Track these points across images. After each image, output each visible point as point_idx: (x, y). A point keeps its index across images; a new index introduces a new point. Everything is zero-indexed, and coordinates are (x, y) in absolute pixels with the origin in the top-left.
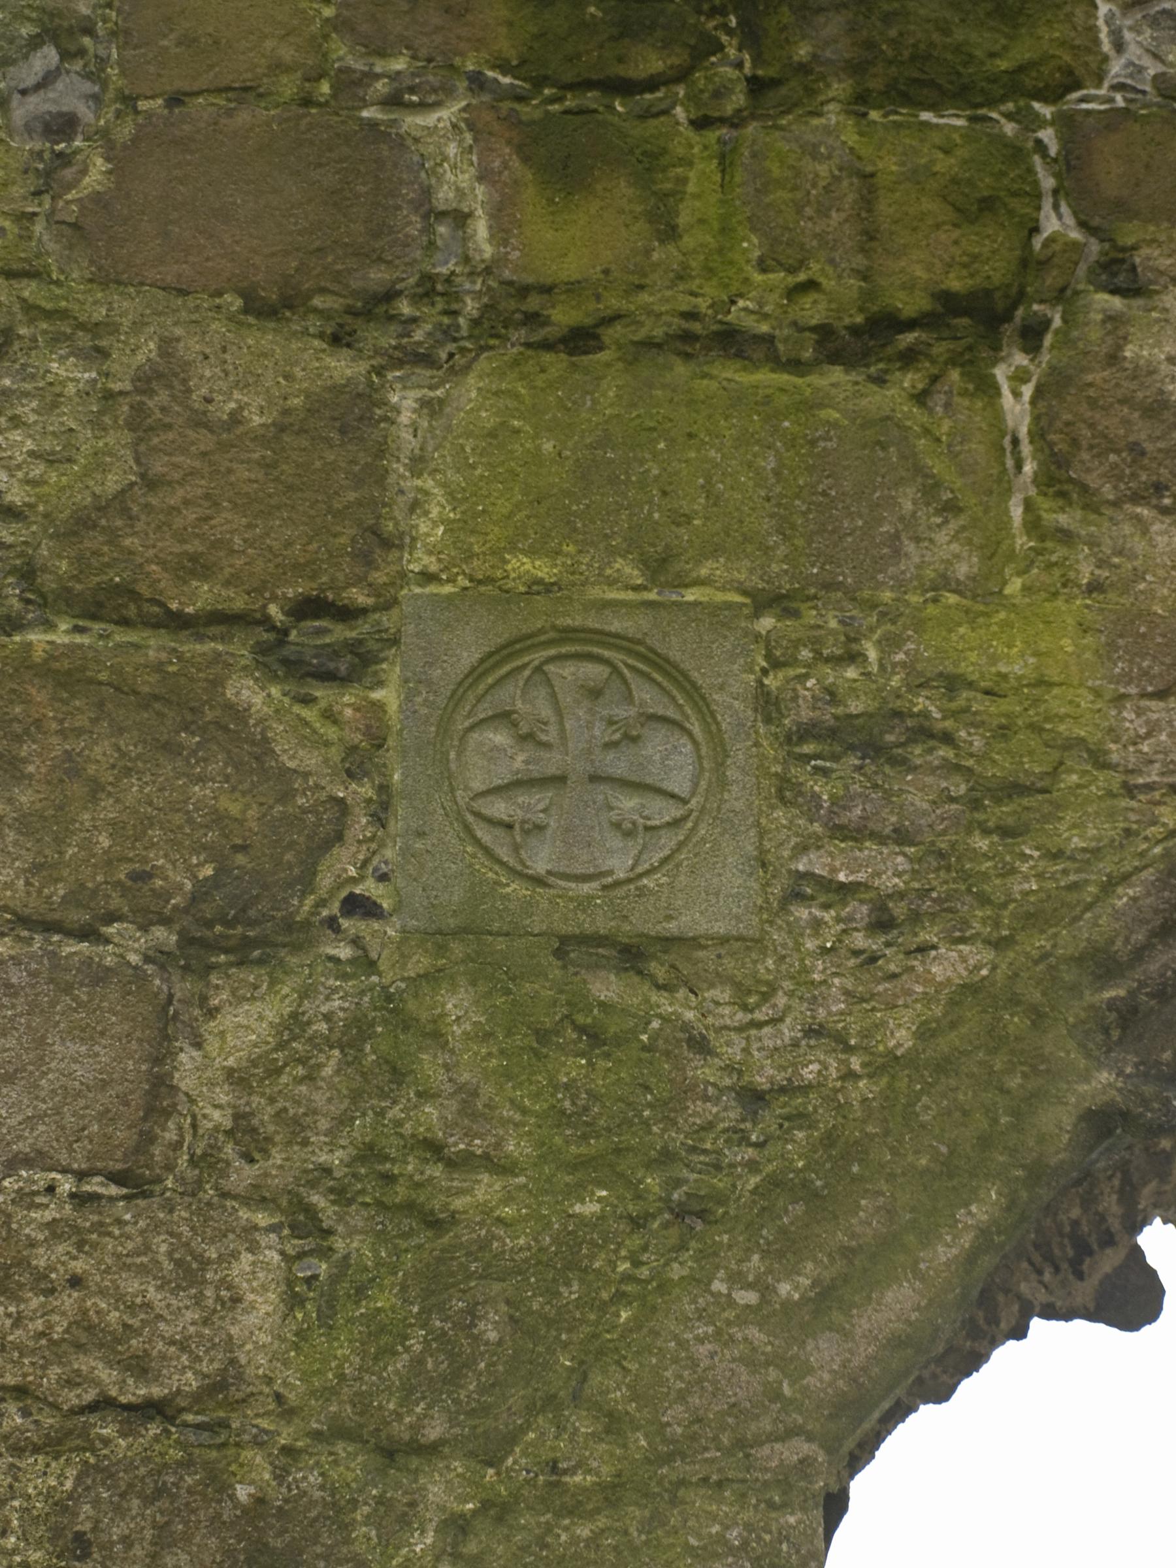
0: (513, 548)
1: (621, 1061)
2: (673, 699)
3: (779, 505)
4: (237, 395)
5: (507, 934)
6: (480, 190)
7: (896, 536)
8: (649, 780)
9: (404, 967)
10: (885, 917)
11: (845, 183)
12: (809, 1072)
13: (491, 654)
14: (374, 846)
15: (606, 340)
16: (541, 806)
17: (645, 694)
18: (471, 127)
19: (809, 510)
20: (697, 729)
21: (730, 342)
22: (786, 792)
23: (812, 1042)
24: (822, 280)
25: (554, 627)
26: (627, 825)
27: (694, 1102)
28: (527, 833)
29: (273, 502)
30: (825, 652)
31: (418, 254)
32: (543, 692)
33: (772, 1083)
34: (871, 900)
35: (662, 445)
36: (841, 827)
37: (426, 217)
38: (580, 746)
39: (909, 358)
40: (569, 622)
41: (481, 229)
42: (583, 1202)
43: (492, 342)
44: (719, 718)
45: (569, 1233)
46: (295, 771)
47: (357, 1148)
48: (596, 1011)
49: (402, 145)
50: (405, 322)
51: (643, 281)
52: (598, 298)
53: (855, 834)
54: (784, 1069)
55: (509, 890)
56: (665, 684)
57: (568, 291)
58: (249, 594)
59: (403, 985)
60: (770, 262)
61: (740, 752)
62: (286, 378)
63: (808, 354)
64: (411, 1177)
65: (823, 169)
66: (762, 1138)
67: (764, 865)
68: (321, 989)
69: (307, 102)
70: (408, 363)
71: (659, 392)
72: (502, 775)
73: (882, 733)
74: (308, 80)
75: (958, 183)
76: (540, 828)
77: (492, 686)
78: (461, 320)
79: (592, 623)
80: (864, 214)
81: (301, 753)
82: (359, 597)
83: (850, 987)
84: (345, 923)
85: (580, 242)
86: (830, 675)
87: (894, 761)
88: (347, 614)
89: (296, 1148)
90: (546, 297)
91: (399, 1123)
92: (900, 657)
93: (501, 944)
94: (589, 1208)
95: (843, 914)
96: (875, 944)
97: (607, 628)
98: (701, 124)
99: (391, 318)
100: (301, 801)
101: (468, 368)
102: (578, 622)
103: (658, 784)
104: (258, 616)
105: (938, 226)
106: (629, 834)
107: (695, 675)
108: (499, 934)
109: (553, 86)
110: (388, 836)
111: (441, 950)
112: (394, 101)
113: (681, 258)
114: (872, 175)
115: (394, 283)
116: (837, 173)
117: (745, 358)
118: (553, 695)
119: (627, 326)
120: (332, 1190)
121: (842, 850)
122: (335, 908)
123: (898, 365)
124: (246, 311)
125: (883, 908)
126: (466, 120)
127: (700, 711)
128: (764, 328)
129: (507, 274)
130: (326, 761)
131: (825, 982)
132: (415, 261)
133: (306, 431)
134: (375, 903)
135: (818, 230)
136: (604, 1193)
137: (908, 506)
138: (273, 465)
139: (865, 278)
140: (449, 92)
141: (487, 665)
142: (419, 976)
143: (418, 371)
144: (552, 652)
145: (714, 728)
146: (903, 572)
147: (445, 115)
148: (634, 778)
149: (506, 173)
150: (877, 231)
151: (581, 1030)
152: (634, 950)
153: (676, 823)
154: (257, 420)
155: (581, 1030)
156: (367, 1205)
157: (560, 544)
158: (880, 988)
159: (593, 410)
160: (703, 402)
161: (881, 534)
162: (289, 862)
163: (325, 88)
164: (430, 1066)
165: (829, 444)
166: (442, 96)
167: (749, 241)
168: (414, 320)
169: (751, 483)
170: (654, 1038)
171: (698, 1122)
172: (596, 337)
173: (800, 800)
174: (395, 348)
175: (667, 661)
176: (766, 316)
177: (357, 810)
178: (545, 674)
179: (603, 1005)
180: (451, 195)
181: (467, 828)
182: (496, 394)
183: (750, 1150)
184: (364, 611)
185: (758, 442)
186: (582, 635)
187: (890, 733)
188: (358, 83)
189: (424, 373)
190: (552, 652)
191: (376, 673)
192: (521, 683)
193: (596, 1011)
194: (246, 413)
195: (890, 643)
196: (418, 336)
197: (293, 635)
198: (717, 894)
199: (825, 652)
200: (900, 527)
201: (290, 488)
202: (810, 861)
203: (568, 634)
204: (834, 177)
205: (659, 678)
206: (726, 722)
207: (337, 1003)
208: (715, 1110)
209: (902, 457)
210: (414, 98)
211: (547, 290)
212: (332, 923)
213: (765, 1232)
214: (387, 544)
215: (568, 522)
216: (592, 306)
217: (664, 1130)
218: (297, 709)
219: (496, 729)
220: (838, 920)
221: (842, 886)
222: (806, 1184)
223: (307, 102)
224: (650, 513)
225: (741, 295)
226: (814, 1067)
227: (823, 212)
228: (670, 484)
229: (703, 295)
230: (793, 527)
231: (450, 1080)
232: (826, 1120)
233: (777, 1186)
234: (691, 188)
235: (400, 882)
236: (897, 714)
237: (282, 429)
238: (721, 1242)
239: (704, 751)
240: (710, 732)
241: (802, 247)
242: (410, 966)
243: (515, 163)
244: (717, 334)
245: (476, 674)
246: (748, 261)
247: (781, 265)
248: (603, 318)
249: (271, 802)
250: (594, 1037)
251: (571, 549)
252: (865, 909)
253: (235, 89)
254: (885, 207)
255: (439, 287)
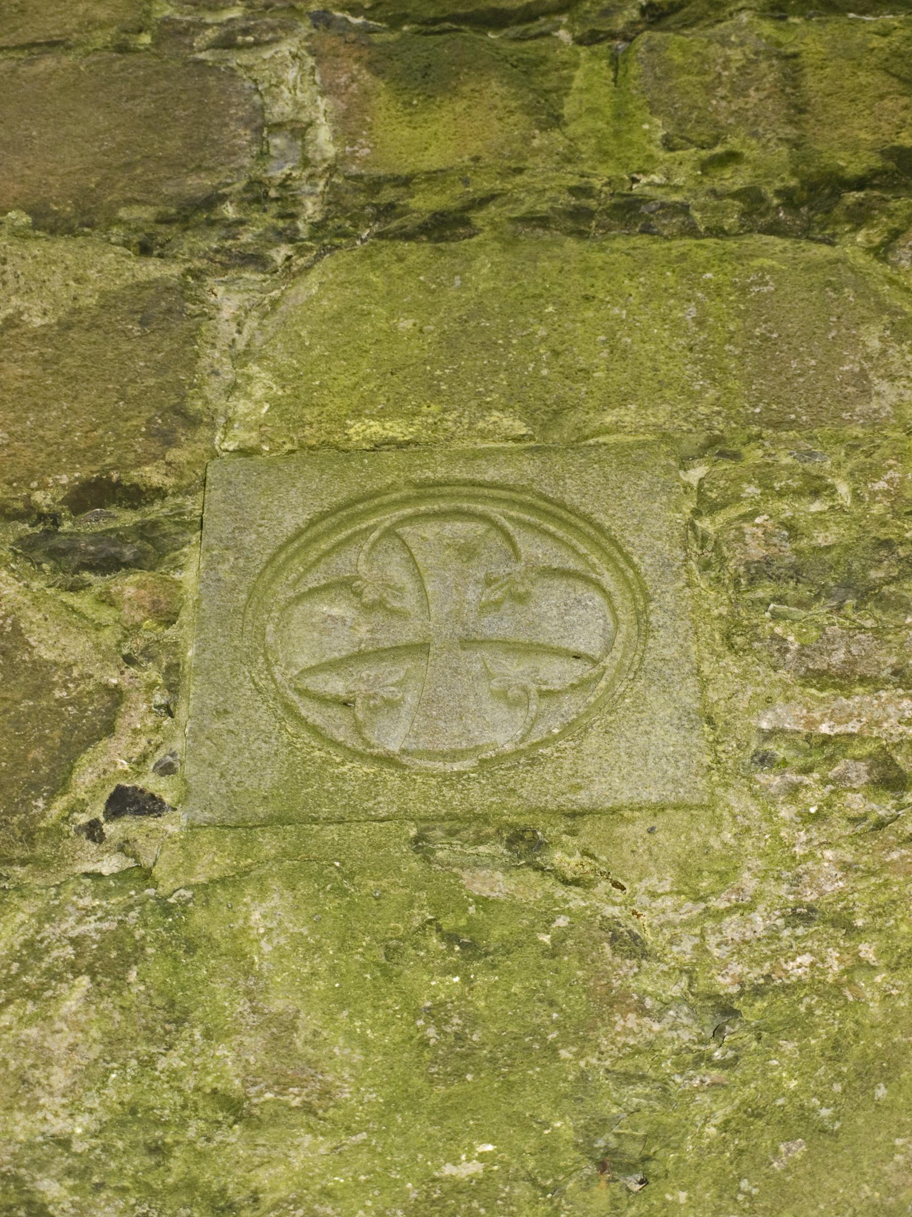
0: (357, 414)
1: (511, 973)
2: (574, 550)
3: (704, 351)
4: (15, 301)
5: (341, 821)
6: (323, 103)
7: (863, 374)
8: (542, 639)
9: (190, 871)
10: (893, 774)
11: (764, 65)
12: (798, 967)
13: (323, 516)
14: (158, 738)
15: (479, 223)
16: (395, 679)
17: (534, 549)
18: (313, 52)
19: (744, 353)
20: (608, 580)
21: (630, 212)
22: (734, 637)
23: (800, 931)
24: (746, 152)
25: (409, 482)
26: (514, 693)
27: (624, 1017)
28: (374, 710)
29: (50, 394)
30: (777, 485)
31: (247, 161)
32: (397, 557)
33: (742, 984)
34: (870, 755)
35: (550, 309)
36: (820, 674)
37: (258, 130)
38: (446, 609)
39: (860, 217)
40: (430, 474)
41: (323, 134)
42: (456, 1161)
43: (337, 241)
44: (636, 559)
45: (434, 1203)
46: (56, 664)
47: (110, 1110)
48: (472, 910)
49: (233, 76)
50: (230, 225)
51: (521, 165)
52: (466, 182)
53: (841, 680)
54: (759, 964)
55: (344, 769)
56: (560, 533)
57: (427, 180)
58: (10, 483)
59: (189, 894)
60: (677, 140)
61: (668, 594)
62: (77, 280)
63: (731, 221)
64: (191, 1143)
65: (736, 55)
66: (730, 1054)
67: (710, 721)
68: (70, 909)
69: (123, 49)
70: (234, 267)
71: (546, 264)
72: (340, 646)
73: (864, 568)
74: (126, 32)
75: (901, 56)
76: (391, 705)
77: (327, 553)
78: (300, 225)
79: (460, 473)
80: (789, 90)
81: (63, 641)
82: (153, 475)
83: (849, 858)
84: (110, 829)
85: (443, 138)
86: (786, 509)
87: (883, 602)
88: (136, 496)
89: (19, 1116)
90: (403, 190)
91: (174, 1075)
92: (881, 485)
93: (332, 833)
94: (467, 1169)
95: (831, 775)
96: (884, 807)
97: (479, 477)
98: (590, 39)
99: (211, 223)
100: (58, 694)
101: (306, 270)
102: (441, 473)
103: (555, 644)
104: (19, 505)
105: (882, 97)
106: (514, 704)
107: (600, 517)
108: (328, 821)
109: (413, 22)
110: (177, 725)
111: (246, 844)
112: (227, 43)
113: (567, 142)
114: (795, 56)
115: (216, 188)
116: (752, 56)
117: (653, 234)
118: (412, 558)
119: (504, 205)
120: (69, 1172)
121: (822, 701)
122: (98, 811)
123: (847, 228)
124: (35, 226)
125: (889, 762)
126: (308, 49)
127: (612, 559)
128: (677, 198)
129: (354, 169)
130: (97, 646)
131: (812, 855)
132: (243, 167)
133: (98, 327)
134: (152, 797)
135: (733, 108)
136: (490, 1148)
137: (875, 344)
138: (56, 360)
139: (797, 146)
140: (288, 29)
141: (321, 527)
142: (213, 881)
143: (247, 275)
144: (408, 511)
145: (630, 574)
146: (875, 411)
147: (286, 47)
148: (523, 638)
149: (354, 86)
150: (807, 103)
151: (451, 938)
152: (528, 835)
153: (583, 685)
154: (38, 322)
155: (451, 938)
156: (125, 1190)
157: (419, 406)
158: (895, 856)
159: (463, 288)
160: (602, 268)
161: (841, 373)
162: (35, 760)
163: (146, 39)
164: (224, 996)
165: (765, 289)
166: (280, 33)
167: (650, 123)
168: (241, 222)
169: (666, 334)
170: (560, 939)
171: (632, 1042)
172: (466, 223)
173: (756, 645)
174: (217, 251)
175: (562, 505)
176: (677, 189)
177: (134, 695)
178: (398, 536)
179: (483, 902)
180: (288, 109)
181: (289, 708)
182: (341, 284)
183: (715, 1072)
184: (160, 493)
185: (673, 296)
186: (447, 489)
187: (877, 568)
188: (185, 32)
189: (250, 275)
190: (408, 511)
191: (175, 559)
192: (366, 547)
193: (472, 910)
194: (25, 317)
195: (865, 473)
196: (246, 238)
197: (66, 526)
198: (645, 755)
199: (777, 485)
200: (866, 365)
201: (73, 378)
202: (778, 717)
203: (426, 489)
204: (749, 60)
205: (552, 528)
206: (645, 564)
207: (93, 925)
208: (656, 1027)
209: (859, 295)
210: (250, 39)
211: (405, 182)
212: (93, 831)
213: (744, 1184)
214: (192, 422)
215: (430, 387)
216: (459, 189)
217: (579, 1055)
218: (66, 597)
219: (332, 601)
220: (824, 782)
221: (826, 740)
222: (804, 1114)
223: (123, 49)
224: (537, 370)
225: (645, 172)
226: (806, 959)
227: (739, 91)
228: (563, 343)
229: (596, 175)
230: (724, 370)
231: (254, 1011)
232: (828, 1022)
233: (759, 1116)
234: (577, 83)
235: (189, 769)
236: (887, 544)
237: (69, 327)
238: (675, 1203)
239: (618, 600)
240: (626, 580)
241: (716, 124)
242: (198, 869)
243: (366, 77)
244: (616, 207)
245: (303, 539)
246: (651, 141)
247: (689, 140)
248: (474, 200)
249: (18, 696)
250: (469, 947)
251: (434, 408)
252: (862, 767)
253: (40, 44)
254: (811, 82)
255: (273, 193)
